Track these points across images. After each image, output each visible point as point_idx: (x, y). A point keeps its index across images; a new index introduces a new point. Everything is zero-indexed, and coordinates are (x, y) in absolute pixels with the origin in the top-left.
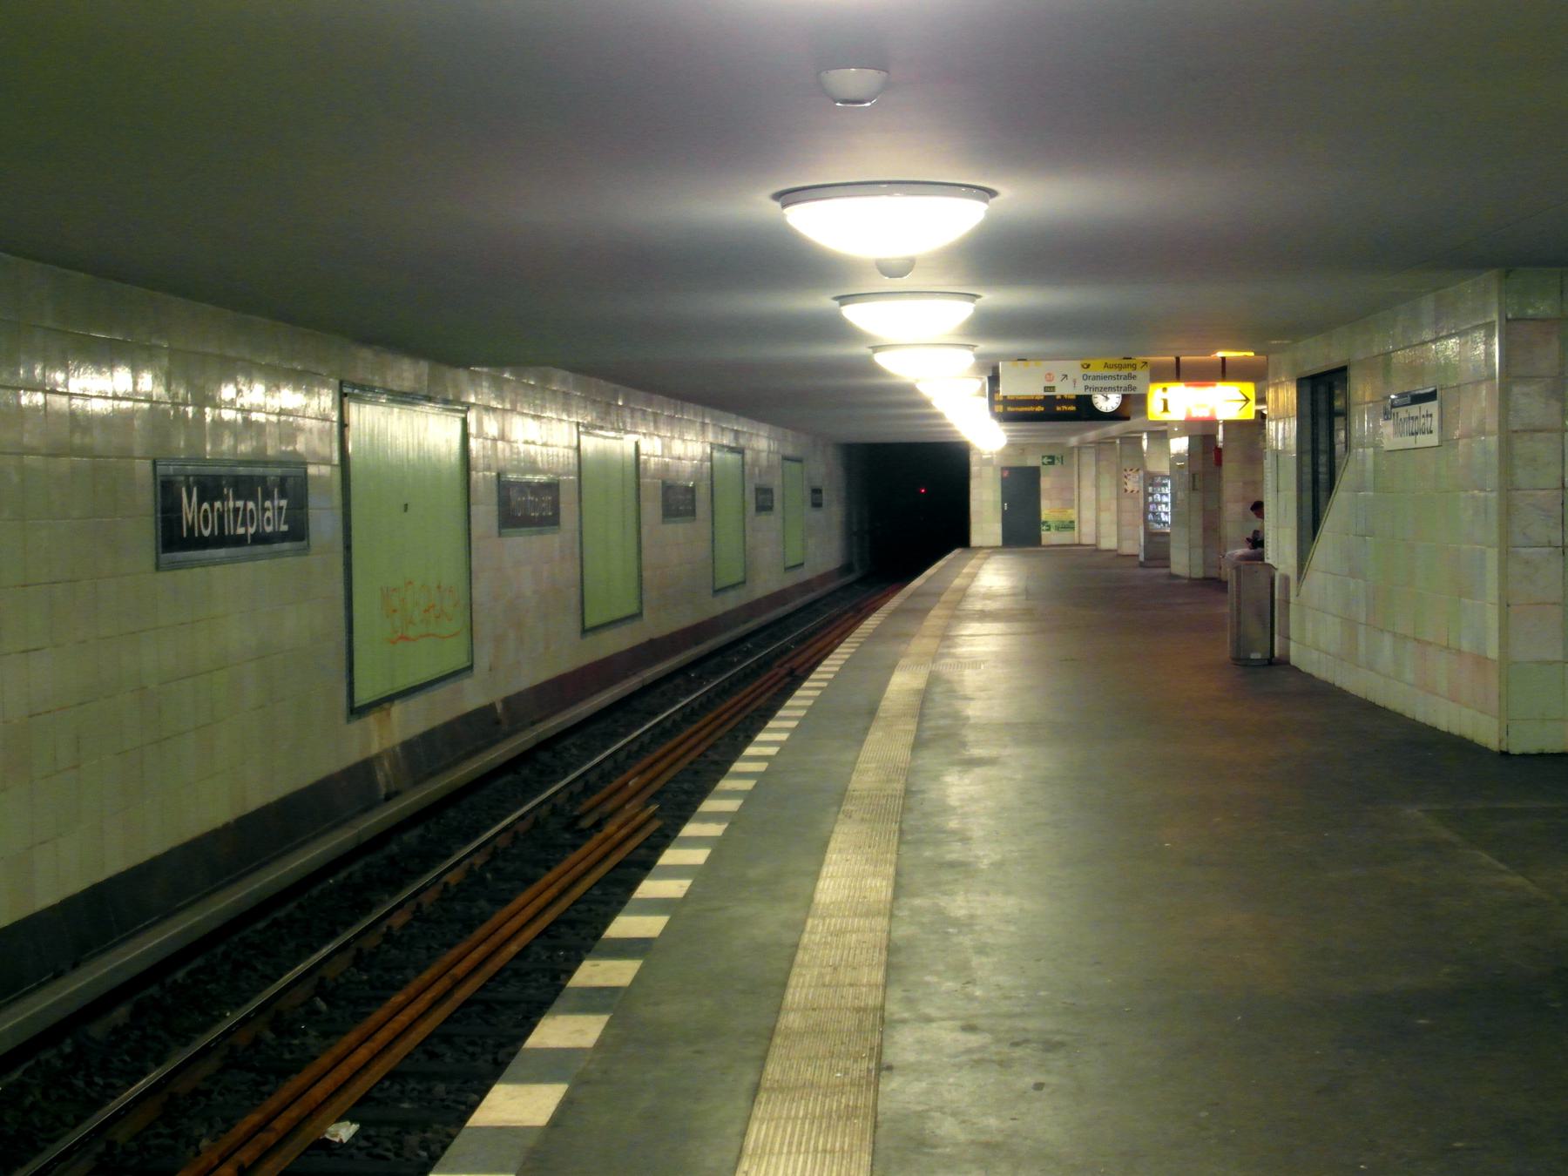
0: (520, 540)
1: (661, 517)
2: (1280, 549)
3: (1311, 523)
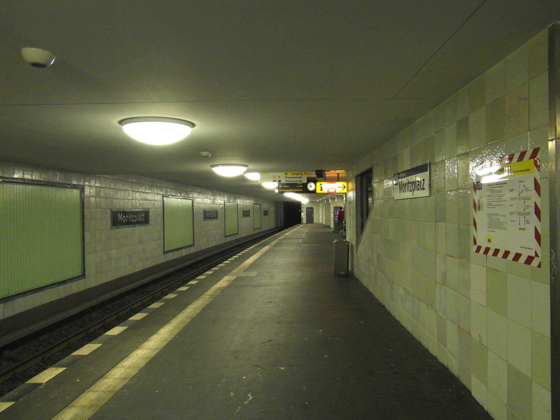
0: (130, 228)
1: (203, 219)
2: (350, 235)
3: (361, 227)
